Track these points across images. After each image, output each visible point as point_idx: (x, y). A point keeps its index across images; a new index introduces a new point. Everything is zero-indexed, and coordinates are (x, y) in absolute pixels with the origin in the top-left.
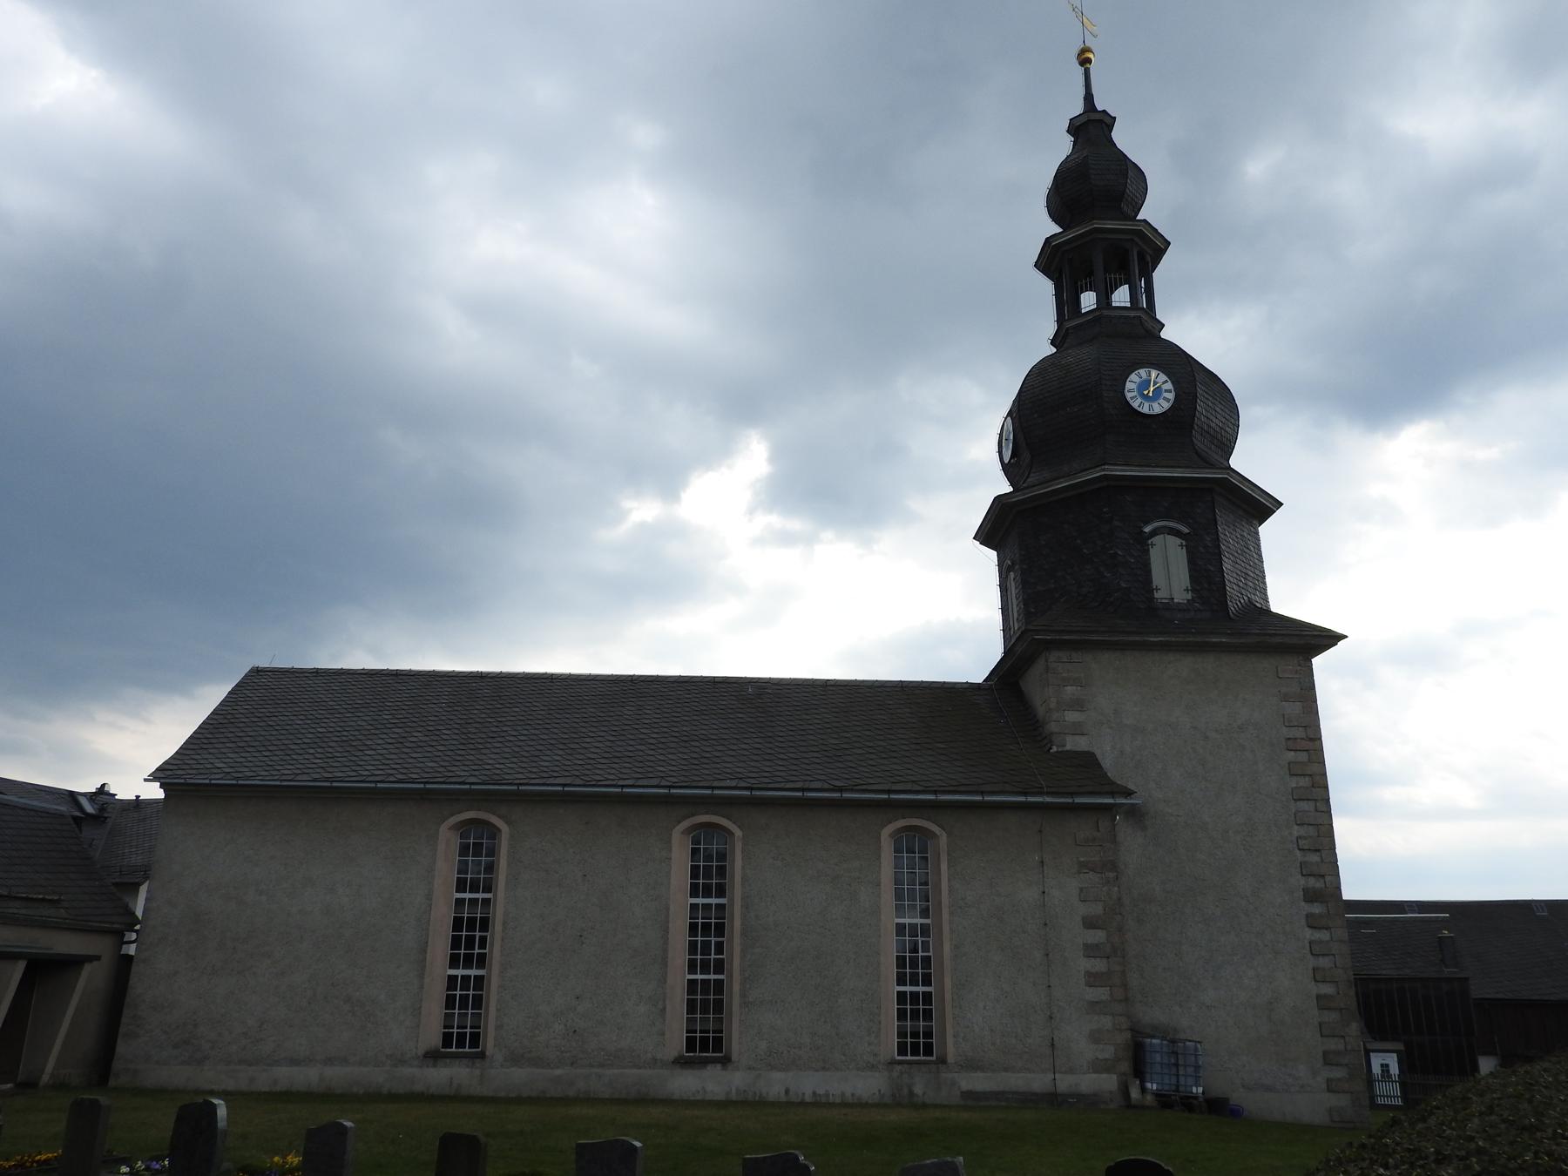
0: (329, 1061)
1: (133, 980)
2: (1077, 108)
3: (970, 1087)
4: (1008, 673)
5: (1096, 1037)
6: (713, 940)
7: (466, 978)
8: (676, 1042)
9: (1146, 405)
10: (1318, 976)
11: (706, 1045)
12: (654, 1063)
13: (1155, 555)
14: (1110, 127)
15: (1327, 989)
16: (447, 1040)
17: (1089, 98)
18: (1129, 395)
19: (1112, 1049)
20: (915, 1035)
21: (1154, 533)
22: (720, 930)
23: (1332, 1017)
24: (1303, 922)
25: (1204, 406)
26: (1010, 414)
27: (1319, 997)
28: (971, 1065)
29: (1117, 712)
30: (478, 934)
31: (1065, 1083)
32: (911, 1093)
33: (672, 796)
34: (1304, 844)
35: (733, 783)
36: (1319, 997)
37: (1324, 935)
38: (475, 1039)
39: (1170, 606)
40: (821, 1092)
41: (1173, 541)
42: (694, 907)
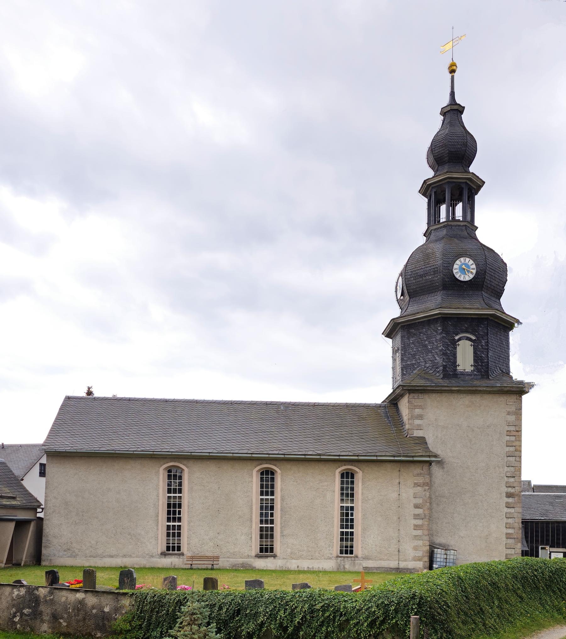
0: (125, 556)
1: (45, 527)
2: (445, 101)
3: (366, 566)
4: (393, 401)
5: (416, 548)
6: (269, 512)
7: (174, 526)
8: (255, 549)
9: (462, 276)
10: (508, 526)
11: (266, 550)
12: (248, 556)
13: (459, 350)
14: (462, 112)
15: (510, 531)
16: (168, 548)
17: (452, 94)
18: (455, 271)
19: (421, 552)
20: (347, 547)
21: (460, 339)
22: (272, 508)
23: (510, 541)
24: (504, 505)
25: (491, 275)
26: (401, 275)
27: (507, 534)
28: (366, 558)
29: (437, 421)
30: (177, 510)
31: (403, 565)
32: (344, 568)
33: (253, 457)
34: (509, 475)
35: (277, 452)
36: (507, 534)
37: (512, 510)
38: (179, 548)
39: (463, 374)
40: (310, 567)
41: (469, 343)
42: (262, 500)
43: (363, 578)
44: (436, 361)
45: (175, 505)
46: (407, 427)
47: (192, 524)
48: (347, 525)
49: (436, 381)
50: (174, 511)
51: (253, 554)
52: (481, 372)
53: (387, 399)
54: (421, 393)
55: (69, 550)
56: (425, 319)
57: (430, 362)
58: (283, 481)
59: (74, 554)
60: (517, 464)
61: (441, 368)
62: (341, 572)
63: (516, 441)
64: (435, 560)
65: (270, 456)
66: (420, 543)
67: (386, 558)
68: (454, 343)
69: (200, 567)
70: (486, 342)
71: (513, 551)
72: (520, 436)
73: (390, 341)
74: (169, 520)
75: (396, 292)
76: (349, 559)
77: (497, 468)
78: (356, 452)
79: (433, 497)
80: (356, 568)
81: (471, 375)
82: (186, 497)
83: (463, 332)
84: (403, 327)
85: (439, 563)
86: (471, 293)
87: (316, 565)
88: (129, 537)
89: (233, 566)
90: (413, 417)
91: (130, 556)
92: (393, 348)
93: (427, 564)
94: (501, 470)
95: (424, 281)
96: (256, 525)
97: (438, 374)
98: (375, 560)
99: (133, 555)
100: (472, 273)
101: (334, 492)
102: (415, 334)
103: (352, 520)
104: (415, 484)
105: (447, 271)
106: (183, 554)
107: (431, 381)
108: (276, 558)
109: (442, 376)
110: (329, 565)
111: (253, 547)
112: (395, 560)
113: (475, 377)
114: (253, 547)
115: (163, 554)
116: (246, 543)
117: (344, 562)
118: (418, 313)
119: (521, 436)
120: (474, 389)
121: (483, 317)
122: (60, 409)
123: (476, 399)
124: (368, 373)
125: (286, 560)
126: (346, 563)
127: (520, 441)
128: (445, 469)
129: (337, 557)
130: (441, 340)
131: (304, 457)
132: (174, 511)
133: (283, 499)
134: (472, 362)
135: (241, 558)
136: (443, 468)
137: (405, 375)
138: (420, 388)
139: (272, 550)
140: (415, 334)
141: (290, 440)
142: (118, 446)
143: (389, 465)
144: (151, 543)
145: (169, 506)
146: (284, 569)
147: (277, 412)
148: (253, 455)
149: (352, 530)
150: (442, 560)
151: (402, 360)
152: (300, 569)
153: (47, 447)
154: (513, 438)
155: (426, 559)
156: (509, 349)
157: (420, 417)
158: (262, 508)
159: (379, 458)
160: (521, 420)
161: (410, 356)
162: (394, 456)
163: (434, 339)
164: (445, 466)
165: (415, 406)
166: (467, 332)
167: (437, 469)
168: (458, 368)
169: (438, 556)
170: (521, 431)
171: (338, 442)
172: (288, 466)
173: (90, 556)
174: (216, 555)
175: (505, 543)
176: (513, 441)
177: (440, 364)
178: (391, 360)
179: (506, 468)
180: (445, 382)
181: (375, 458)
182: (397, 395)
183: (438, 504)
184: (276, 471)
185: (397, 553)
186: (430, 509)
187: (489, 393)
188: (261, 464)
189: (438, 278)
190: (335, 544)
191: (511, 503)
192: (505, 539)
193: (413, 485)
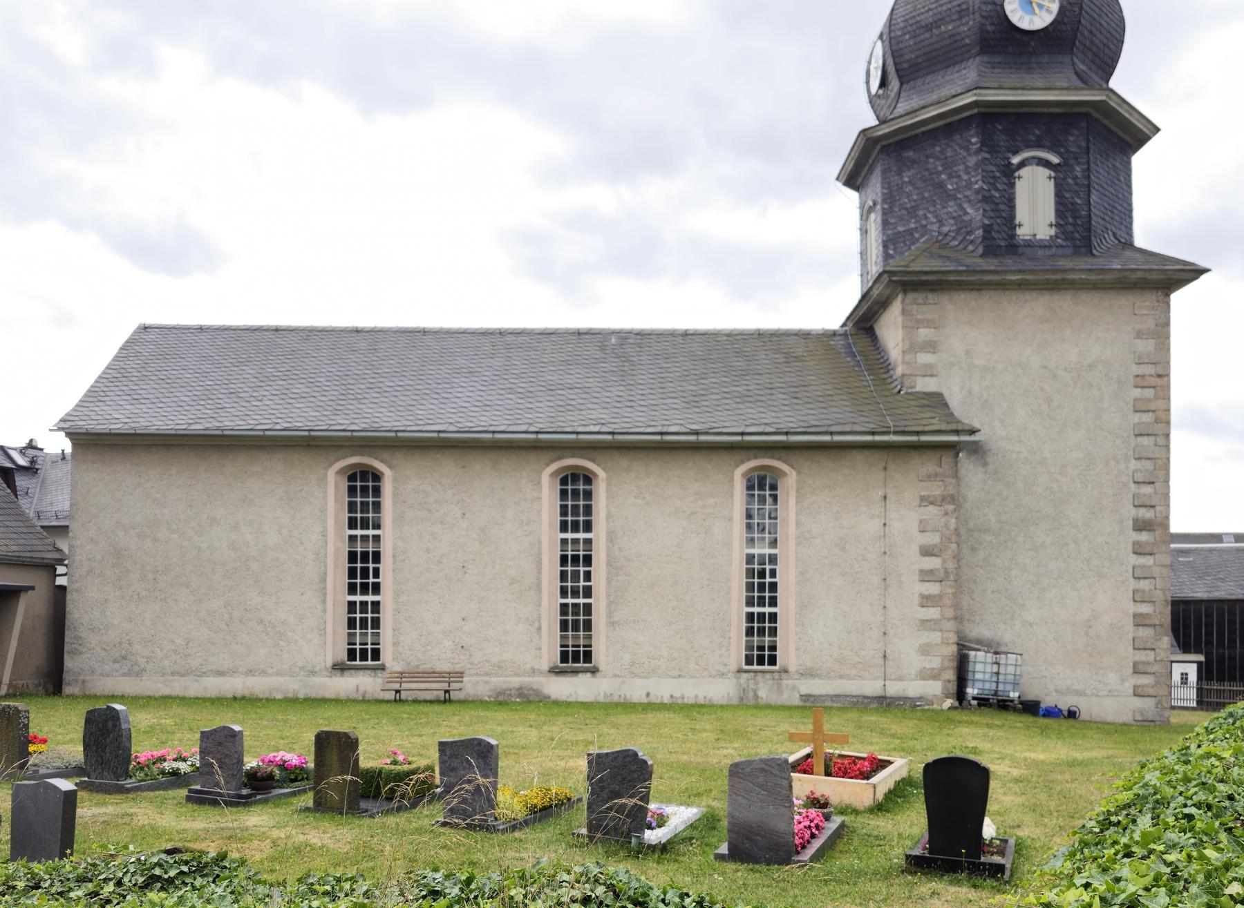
0: (250, 672)
1: (70, 607)
4: (865, 320)
5: (925, 650)
8: (550, 651)
11: (576, 657)
12: (534, 671)
15: (1145, 609)
16: (351, 654)
20: (761, 648)
21: (1022, 164)
23: (1145, 633)
26: (881, 37)
27: (1135, 616)
29: (967, 356)
31: (894, 689)
32: (756, 697)
33: (540, 441)
36: (1135, 616)
37: (1148, 561)
38: (376, 654)
39: (1031, 244)
40: (677, 694)
43: (818, 728)
44: (966, 218)
45: (365, 556)
46: (899, 371)
47: (403, 598)
48: (762, 599)
49: (968, 261)
50: (363, 568)
51: (545, 666)
52: (1074, 239)
53: (848, 318)
54: (933, 290)
55: (124, 658)
56: (939, 124)
57: (952, 222)
58: (611, 496)
59: (136, 668)
60: (1159, 453)
61: (980, 232)
62: (748, 707)
63: (1156, 397)
64: (970, 676)
65: (581, 437)
66: (936, 637)
67: (854, 672)
68: (1009, 174)
69: (428, 698)
70: (1084, 171)
71: (1150, 656)
72: (1167, 388)
73: (853, 196)
74: (352, 589)
75: (868, 82)
76: (768, 676)
77: (1112, 463)
78: (784, 427)
79: (963, 531)
80: (785, 696)
81: (1050, 247)
82: (390, 537)
83: (1029, 146)
84: (886, 150)
85: (980, 685)
86: (1046, 58)
87: (691, 690)
88: (260, 628)
89: (499, 694)
90: (912, 348)
91: (264, 673)
92: (862, 207)
93: (953, 687)
94: (1122, 466)
95: (934, 39)
96: (551, 601)
97: (971, 248)
98: (829, 678)
99: (270, 671)
100: (1049, 11)
101: (731, 519)
102: (914, 162)
103: (773, 587)
104: (923, 499)
105: (990, 7)
106: (383, 668)
107: (958, 261)
108: (598, 674)
109: (980, 250)
110: (721, 690)
111: (545, 649)
112: (876, 679)
113: (1060, 251)
114: (545, 649)
115: (339, 668)
116: (530, 644)
117: (756, 683)
118: (924, 107)
119: (1168, 387)
120: (1059, 276)
121: (1076, 110)
122: (121, 349)
123: (1063, 302)
124: (809, 259)
125: (619, 680)
126: (761, 685)
127: (1167, 398)
128: (991, 468)
129: (740, 671)
130: (977, 165)
131: (658, 438)
132: (363, 568)
133: (611, 539)
134: (1051, 216)
135: (516, 675)
136: (985, 464)
137: (892, 257)
138: (930, 278)
139: (588, 656)
140: (914, 162)
141: (629, 404)
142: (233, 420)
143: (859, 457)
144: (310, 641)
145: (352, 557)
146: (616, 699)
147: (603, 349)
148: (540, 436)
149: (772, 610)
150: (987, 677)
151: (885, 223)
152: (653, 699)
153: (71, 423)
154: (1149, 393)
155: (951, 675)
156: (1130, 193)
157: (931, 346)
158: (564, 560)
159: (837, 438)
160: (1169, 350)
161: (904, 212)
162: (873, 433)
163: (961, 167)
164: (990, 460)
165: (918, 321)
166: (1038, 145)
167: (971, 467)
168: (1019, 231)
169: (979, 667)
170: (1168, 375)
171: (740, 406)
172: (624, 461)
173: (173, 674)
174: (458, 668)
175: (1131, 636)
176: (1149, 400)
177: (976, 224)
178: (856, 236)
179: (1133, 461)
180: (991, 264)
181: (827, 438)
182: (876, 302)
183: (973, 549)
184: (596, 475)
185: (881, 661)
186: (957, 557)
187: (1094, 287)
188: (560, 458)
189: (968, 27)
190: (734, 641)
191: (1147, 543)
192: (1131, 627)
193: (917, 502)
